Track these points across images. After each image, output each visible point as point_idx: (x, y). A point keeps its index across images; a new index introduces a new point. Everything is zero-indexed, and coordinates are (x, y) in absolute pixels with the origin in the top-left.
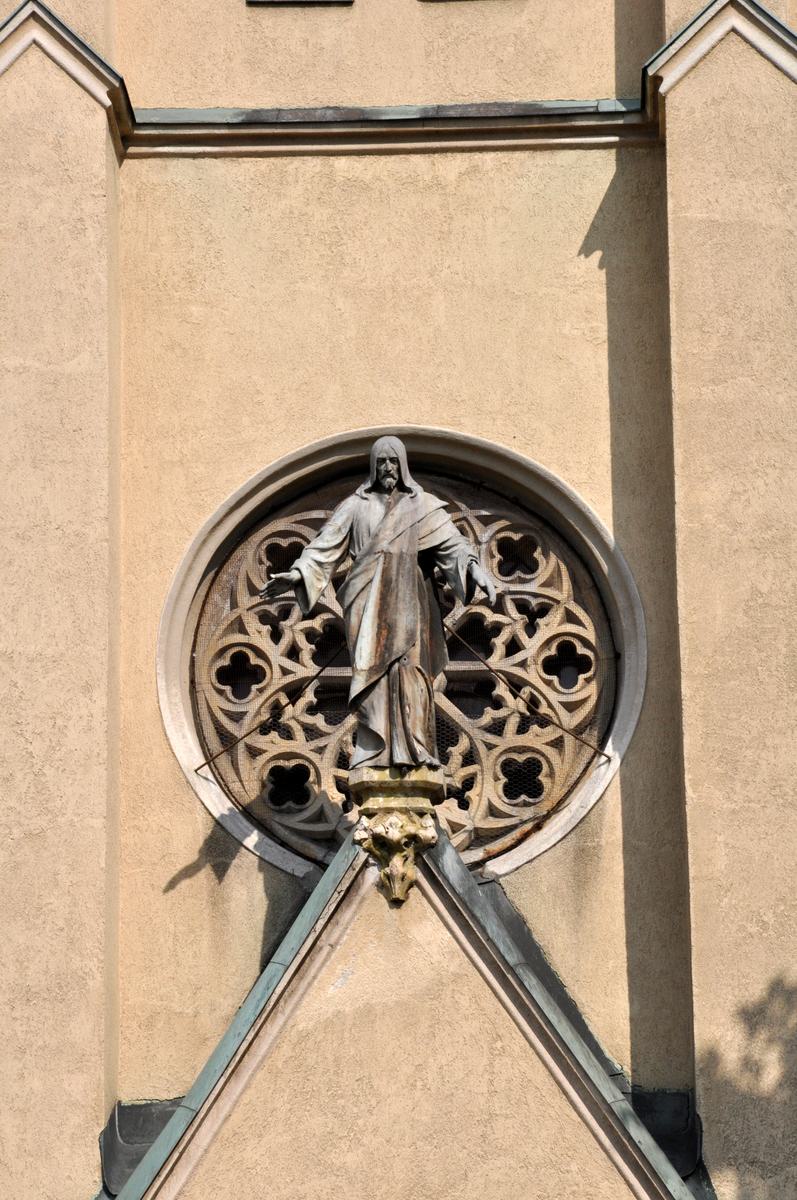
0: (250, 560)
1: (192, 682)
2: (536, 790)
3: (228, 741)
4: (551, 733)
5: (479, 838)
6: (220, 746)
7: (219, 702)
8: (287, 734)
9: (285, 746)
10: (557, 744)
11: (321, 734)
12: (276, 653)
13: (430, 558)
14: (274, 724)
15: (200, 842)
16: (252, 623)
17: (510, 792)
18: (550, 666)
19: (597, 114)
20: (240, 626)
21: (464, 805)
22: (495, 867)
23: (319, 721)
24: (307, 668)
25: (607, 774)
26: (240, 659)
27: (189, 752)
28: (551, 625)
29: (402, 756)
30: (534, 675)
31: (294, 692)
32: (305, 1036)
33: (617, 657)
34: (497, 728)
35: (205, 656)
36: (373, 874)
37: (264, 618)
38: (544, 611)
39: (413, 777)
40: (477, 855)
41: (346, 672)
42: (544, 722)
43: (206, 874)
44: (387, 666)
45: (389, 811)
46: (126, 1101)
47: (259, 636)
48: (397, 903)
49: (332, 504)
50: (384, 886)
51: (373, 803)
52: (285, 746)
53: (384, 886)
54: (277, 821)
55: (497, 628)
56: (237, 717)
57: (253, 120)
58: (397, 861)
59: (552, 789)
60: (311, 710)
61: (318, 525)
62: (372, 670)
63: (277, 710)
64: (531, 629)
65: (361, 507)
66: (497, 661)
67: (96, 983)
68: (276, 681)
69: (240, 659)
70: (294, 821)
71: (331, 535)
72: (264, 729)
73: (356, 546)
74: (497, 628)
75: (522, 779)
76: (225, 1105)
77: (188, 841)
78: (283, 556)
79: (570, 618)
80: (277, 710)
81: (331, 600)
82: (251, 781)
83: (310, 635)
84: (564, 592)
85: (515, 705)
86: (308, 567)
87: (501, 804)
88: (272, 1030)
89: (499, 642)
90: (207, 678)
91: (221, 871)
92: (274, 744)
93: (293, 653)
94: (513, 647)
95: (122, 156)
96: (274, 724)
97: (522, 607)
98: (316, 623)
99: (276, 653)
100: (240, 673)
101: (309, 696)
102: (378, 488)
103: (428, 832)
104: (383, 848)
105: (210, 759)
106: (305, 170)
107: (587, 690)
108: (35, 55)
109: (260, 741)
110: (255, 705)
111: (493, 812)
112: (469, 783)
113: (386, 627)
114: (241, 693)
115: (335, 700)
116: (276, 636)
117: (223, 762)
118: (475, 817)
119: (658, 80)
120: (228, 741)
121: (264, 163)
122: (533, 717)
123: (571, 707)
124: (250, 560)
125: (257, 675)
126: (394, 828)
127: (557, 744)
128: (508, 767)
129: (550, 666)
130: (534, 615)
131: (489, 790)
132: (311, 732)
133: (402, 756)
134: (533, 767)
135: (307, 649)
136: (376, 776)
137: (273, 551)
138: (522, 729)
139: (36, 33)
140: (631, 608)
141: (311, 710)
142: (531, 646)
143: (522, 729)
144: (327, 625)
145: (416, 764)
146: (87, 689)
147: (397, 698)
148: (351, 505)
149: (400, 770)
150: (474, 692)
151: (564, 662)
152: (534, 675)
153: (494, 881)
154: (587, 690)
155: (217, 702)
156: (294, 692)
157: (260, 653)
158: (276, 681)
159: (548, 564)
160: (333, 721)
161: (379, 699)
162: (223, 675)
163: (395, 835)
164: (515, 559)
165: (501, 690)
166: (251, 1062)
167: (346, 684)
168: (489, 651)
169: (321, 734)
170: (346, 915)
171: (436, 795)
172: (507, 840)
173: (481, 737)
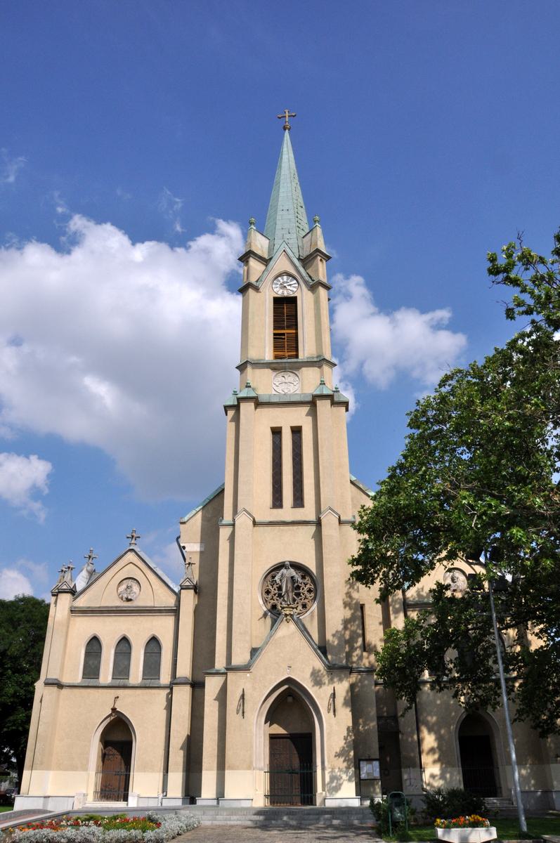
6: (265, 602)
7: (265, 596)
15: (272, 348)
17: (303, 608)
18: (308, 591)
24: (276, 592)
25: (315, 605)
26: (268, 590)
28: (308, 586)
33: (316, 590)
43: (263, 619)
47: (270, 587)
50: (286, 620)
53: (286, 620)
58: (288, 617)
59: (308, 608)
66: (301, 591)
67: (249, 632)
69: (268, 590)
77: (261, 614)
82: (269, 606)
84: (309, 582)
91: (265, 618)
92: (272, 601)
100: (268, 592)
104: (286, 615)
107: (312, 594)
110: (270, 596)
113: (287, 586)
122: (305, 598)
124: (269, 577)
125: (270, 592)
129: (308, 591)
130: (306, 585)
132: (277, 600)
140: (323, 769)
147: (288, 596)
151: (310, 591)
154: (312, 594)
159: (307, 578)
161: (286, 595)
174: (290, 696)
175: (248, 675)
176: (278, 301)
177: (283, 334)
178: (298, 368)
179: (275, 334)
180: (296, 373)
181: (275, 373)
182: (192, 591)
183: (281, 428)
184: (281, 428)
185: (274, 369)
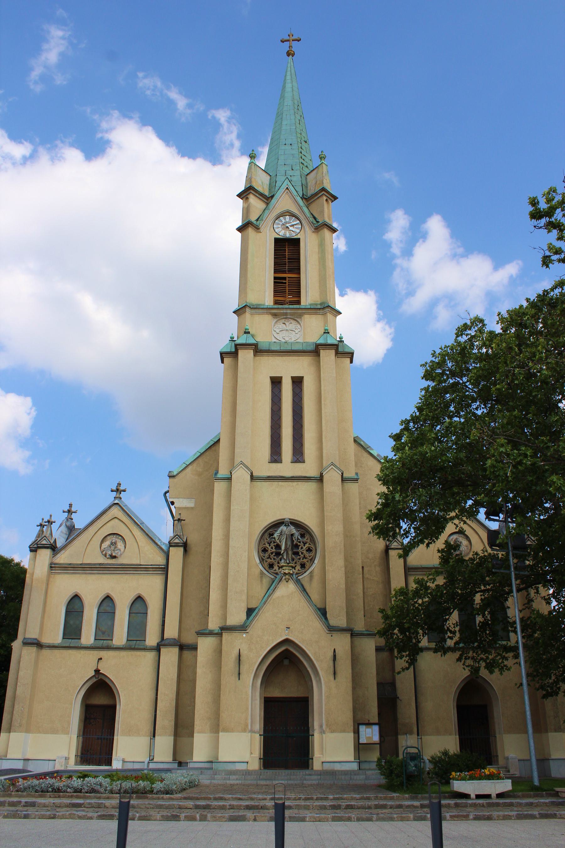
0: (266, 535)
1: (258, 551)
2: (305, 567)
3: (263, 560)
4: (307, 560)
5: (297, 574)
8: (271, 559)
9: (271, 561)
10: (308, 561)
11: (301, 552)
12: (269, 548)
13: (292, 535)
14: (269, 557)
16: (267, 544)
17: (301, 568)
19: (314, 477)
20: (265, 544)
21: (295, 569)
22: (299, 578)
23: (275, 557)
24: (274, 550)
26: (265, 549)
27: (258, 561)
28: (307, 545)
29: (288, 562)
30: (305, 552)
31: (272, 553)
32: (274, 599)
34: (300, 559)
35: (260, 548)
36: (284, 578)
37: (268, 543)
38: (306, 543)
39: (290, 565)
40: (297, 576)
41: (280, 551)
42: (306, 558)
44: (286, 550)
45: (286, 569)
46: (249, 607)
47: (267, 545)
48: (287, 582)
49: (279, 527)
50: (285, 579)
51: (284, 568)
52: (271, 561)
54: (269, 571)
55: (300, 545)
56: (264, 556)
57: (269, 477)
59: (307, 567)
60: (274, 556)
61: (276, 531)
62: (284, 550)
63: (270, 556)
64: (304, 546)
65: (283, 528)
67: (246, 591)
68: (269, 552)
69: (265, 549)
70: (272, 571)
71: (279, 532)
72: (268, 558)
73: (359, 603)
74: (300, 545)
75: (303, 566)
76: (263, 608)
78: (271, 535)
79: (310, 544)
80: (270, 556)
81: (278, 541)
83: (274, 545)
84: (309, 541)
85: (302, 544)
86: (276, 535)
87: (300, 569)
88: (270, 598)
89: (300, 547)
90: (260, 551)
93: (272, 548)
94: (302, 548)
95: (251, 481)
96: (269, 557)
97: (303, 542)
98: (275, 544)
99: (269, 548)
100: (265, 550)
101: (274, 554)
102: (285, 525)
103: (291, 572)
104: (285, 574)
105: (261, 562)
106: (275, 484)
108: (241, 468)
109: (267, 560)
111: (299, 570)
112: (296, 566)
114: (265, 553)
115: (278, 554)
116: (270, 546)
117: (262, 563)
118: (296, 571)
119: (323, 473)
120: (263, 560)
121: (270, 483)
122: (305, 557)
123: (310, 556)
125: (267, 551)
126: (287, 571)
127: (308, 561)
128: (301, 564)
129: (307, 551)
130: (305, 544)
131: (298, 567)
132: (274, 559)
133: (288, 562)
134: (304, 564)
135: (274, 547)
136: (284, 564)
137: (270, 534)
138: (303, 559)
139: (241, 465)
141: (274, 556)
142: (304, 548)
143: (303, 559)
144: (277, 544)
145: (290, 563)
146: (245, 552)
147: (287, 554)
148: (281, 528)
149: (288, 563)
150: (296, 554)
152: (305, 552)
153: (299, 580)
155: (262, 554)
156: (272, 553)
157: (267, 548)
158: (269, 552)
159: (307, 536)
160: (277, 557)
162: (263, 551)
163: (287, 572)
164: (302, 536)
165: (300, 554)
166: (267, 603)
167: (281, 552)
168: (298, 548)
169: (301, 552)
170: (280, 583)
171: (292, 567)
172: (301, 574)
173: (297, 560)
174: (286, 658)
175: (244, 635)
176: (280, 243)
177: (284, 278)
178: (300, 316)
179: (275, 278)
180: (298, 320)
181: (275, 320)
182: (182, 549)
183: (281, 377)
184: (281, 377)
185: (275, 315)
